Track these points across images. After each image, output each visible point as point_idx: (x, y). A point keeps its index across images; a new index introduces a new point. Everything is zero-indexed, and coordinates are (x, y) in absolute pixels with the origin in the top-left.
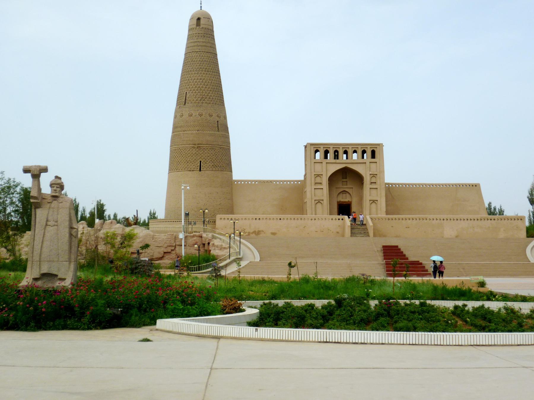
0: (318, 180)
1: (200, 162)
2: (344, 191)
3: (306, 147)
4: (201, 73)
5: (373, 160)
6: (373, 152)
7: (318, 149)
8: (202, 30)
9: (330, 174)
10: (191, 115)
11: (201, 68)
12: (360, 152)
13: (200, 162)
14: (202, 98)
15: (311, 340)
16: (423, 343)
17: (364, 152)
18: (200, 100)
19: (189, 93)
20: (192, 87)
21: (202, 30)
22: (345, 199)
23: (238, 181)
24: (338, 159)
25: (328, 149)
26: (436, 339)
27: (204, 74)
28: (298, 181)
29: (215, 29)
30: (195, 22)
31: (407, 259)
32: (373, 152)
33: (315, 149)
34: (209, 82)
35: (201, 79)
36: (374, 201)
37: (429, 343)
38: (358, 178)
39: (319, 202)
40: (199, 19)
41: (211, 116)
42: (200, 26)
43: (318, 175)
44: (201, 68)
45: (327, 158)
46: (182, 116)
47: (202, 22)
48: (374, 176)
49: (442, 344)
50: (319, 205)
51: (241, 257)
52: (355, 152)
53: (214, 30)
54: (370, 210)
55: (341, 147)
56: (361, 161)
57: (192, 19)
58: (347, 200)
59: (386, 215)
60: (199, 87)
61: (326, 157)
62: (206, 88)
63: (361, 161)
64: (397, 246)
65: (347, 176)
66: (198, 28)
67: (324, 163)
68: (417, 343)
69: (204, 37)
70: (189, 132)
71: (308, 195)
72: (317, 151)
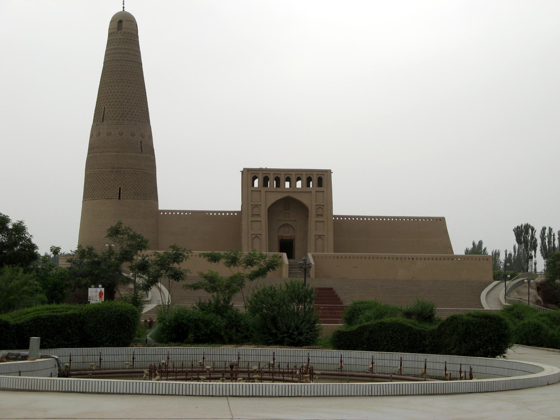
0: (256, 211)
1: (120, 188)
2: (286, 224)
3: (242, 172)
4: (122, 85)
5: (320, 189)
6: (320, 179)
7: (301, 176)
8: (123, 35)
9: (270, 203)
10: (109, 134)
11: (122, 79)
12: (305, 178)
13: (120, 188)
14: (123, 114)
15: (55, 390)
16: (164, 393)
17: (309, 179)
18: (121, 117)
19: (108, 108)
20: (112, 102)
21: (123, 35)
22: (287, 234)
23: (164, 211)
24: (321, 186)
25: (268, 176)
26: (353, 391)
27: (126, 86)
28: (234, 212)
29: (140, 34)
30: (116, 25)
31: (342, 303)
32: (320, 179)
33: (253, 175)
34: (131, 96)
35: (122, 92)
36: (320, 236)
37: (177, 393)
38: (303, 209)
39: (257, 236)
40: (120, 22)
41: (133, 135)
42: (122, 30)
43: (256, 206)
44: (122, 79)
45: (309, 186)
46: (99, 135)
47: (124, 24)
48: (320, 207)
49: (204, 394)
50: (256, 241)
51: (149, 299)
52: (299, 179)
53: (139, 34)
54: (316, 245)
55: (272, 175)
56: (307, 189)
57: (112, 22)
58: (290, 235)
59: (334, 252)
60: (120, 102)
61: (265, 185)
62: (128, 102)
63: (307, 189)
64: (332, 289)
65: (289, 206)
66: (119, 32)
67: (263, 192)
68: (214, 394)
69: (127, 43)
70: (107, 154)
71: (244, 227)
72: (254, 178)
